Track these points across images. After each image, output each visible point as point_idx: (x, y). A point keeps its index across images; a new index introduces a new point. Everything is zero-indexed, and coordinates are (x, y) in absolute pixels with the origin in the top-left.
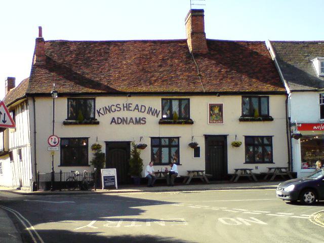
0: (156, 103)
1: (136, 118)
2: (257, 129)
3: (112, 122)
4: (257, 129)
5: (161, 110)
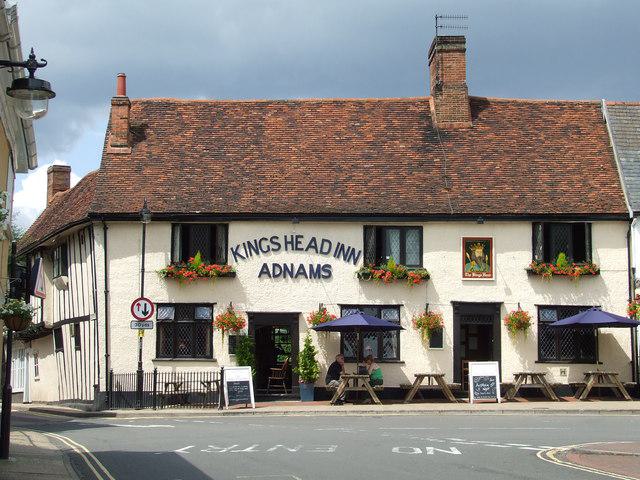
1: (311, 266)
3: (262, 273)
5: (362, 249)
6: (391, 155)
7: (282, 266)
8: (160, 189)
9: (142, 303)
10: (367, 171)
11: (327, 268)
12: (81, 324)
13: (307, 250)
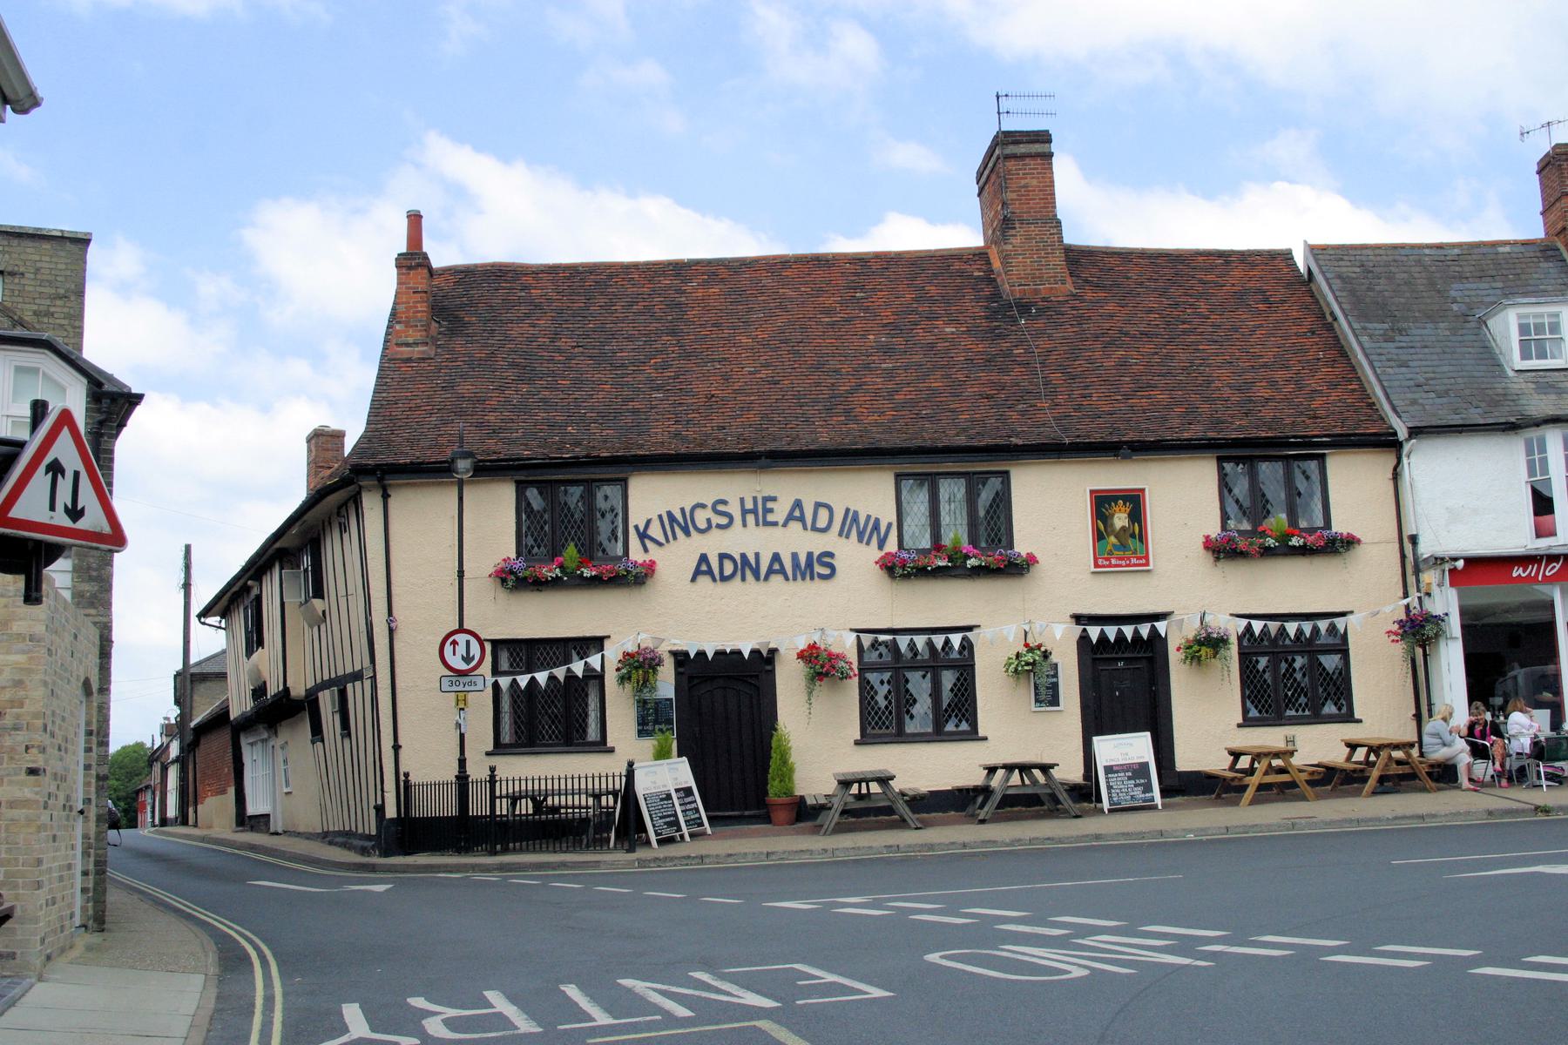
0: (871, 494)
1: (795, 556)
2: (1289, 589)
3: (697, 573)
4: (1289, 589)
5: (893, 518)
6: (932, 346)
7: (738, 558)
8: (491, 417)
9: (461, 638)
10: (890, 374)
11: (826, 558)
12: (349, 686)
13: (785, 525)
